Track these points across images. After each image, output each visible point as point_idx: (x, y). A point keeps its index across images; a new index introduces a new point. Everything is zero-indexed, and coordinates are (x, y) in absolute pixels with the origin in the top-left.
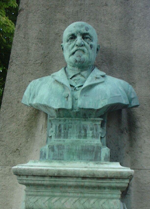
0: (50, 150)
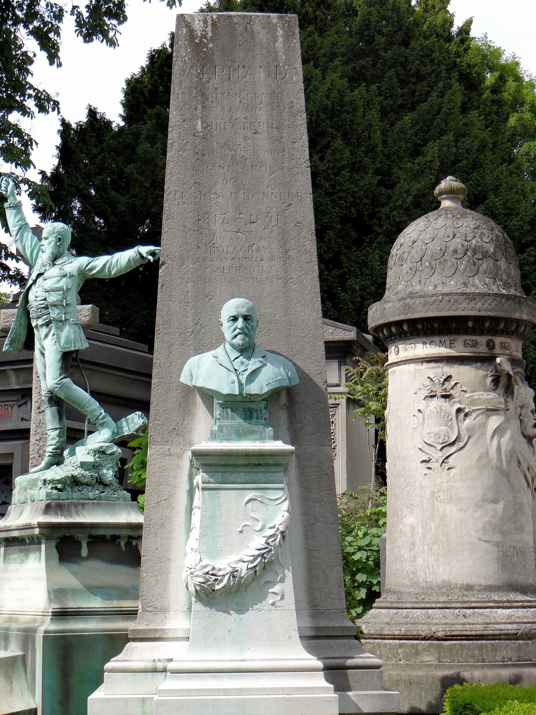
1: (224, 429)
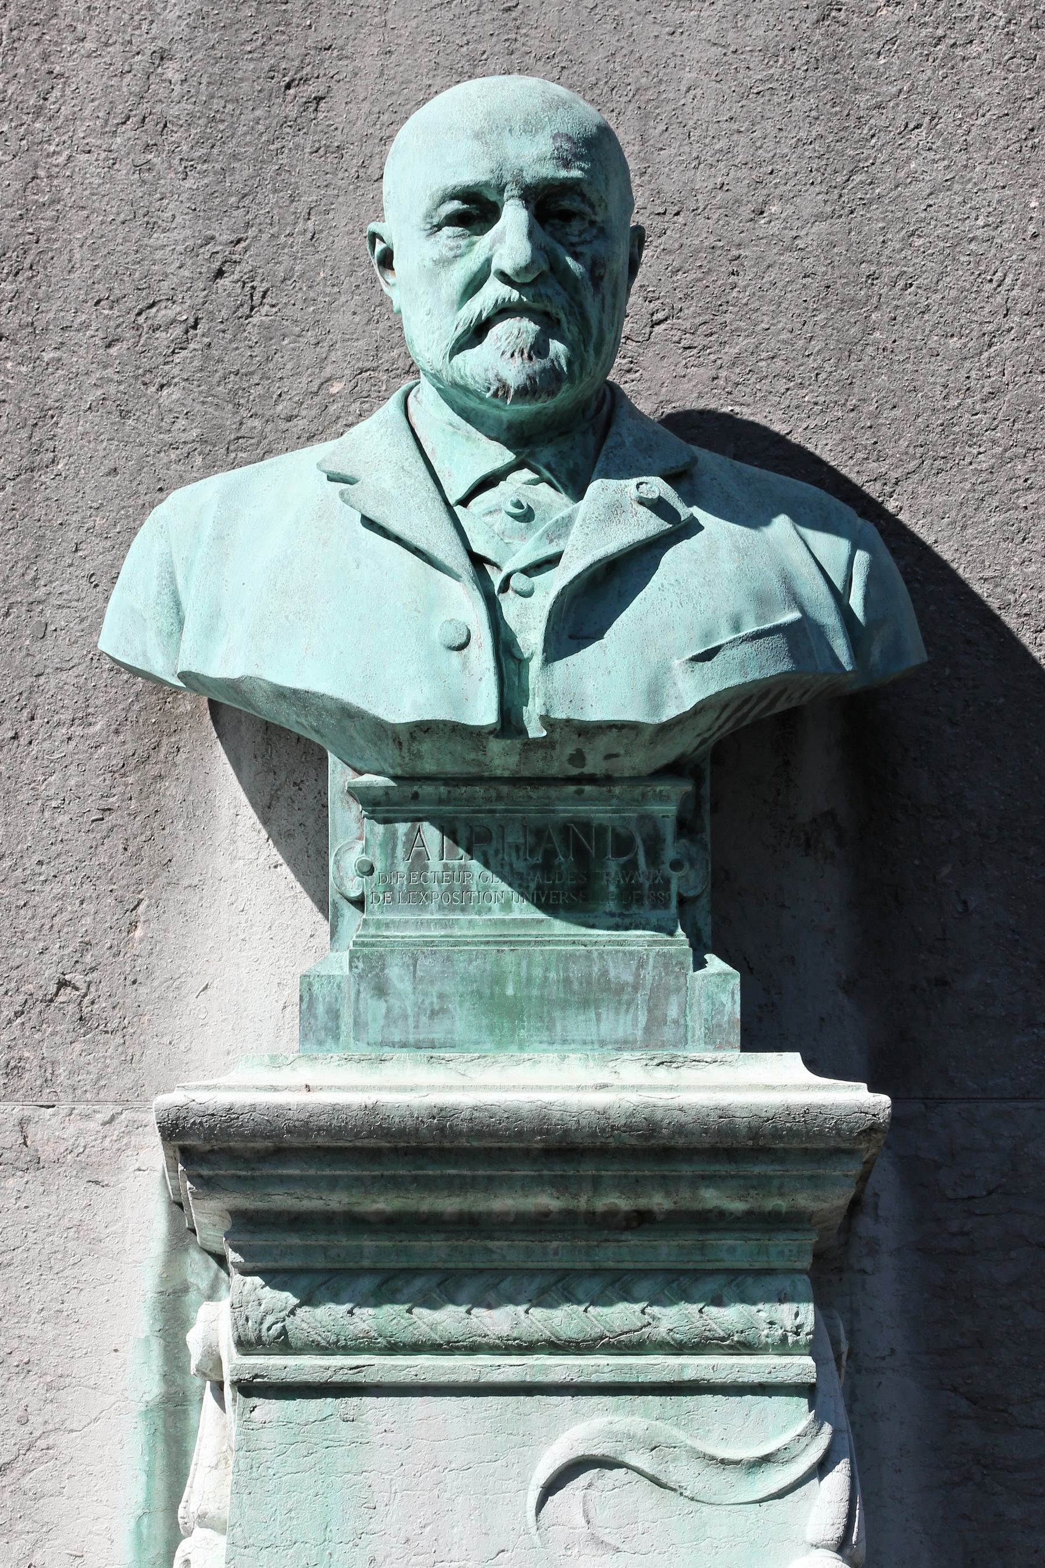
0: (363, 985)
1: (396, 973)
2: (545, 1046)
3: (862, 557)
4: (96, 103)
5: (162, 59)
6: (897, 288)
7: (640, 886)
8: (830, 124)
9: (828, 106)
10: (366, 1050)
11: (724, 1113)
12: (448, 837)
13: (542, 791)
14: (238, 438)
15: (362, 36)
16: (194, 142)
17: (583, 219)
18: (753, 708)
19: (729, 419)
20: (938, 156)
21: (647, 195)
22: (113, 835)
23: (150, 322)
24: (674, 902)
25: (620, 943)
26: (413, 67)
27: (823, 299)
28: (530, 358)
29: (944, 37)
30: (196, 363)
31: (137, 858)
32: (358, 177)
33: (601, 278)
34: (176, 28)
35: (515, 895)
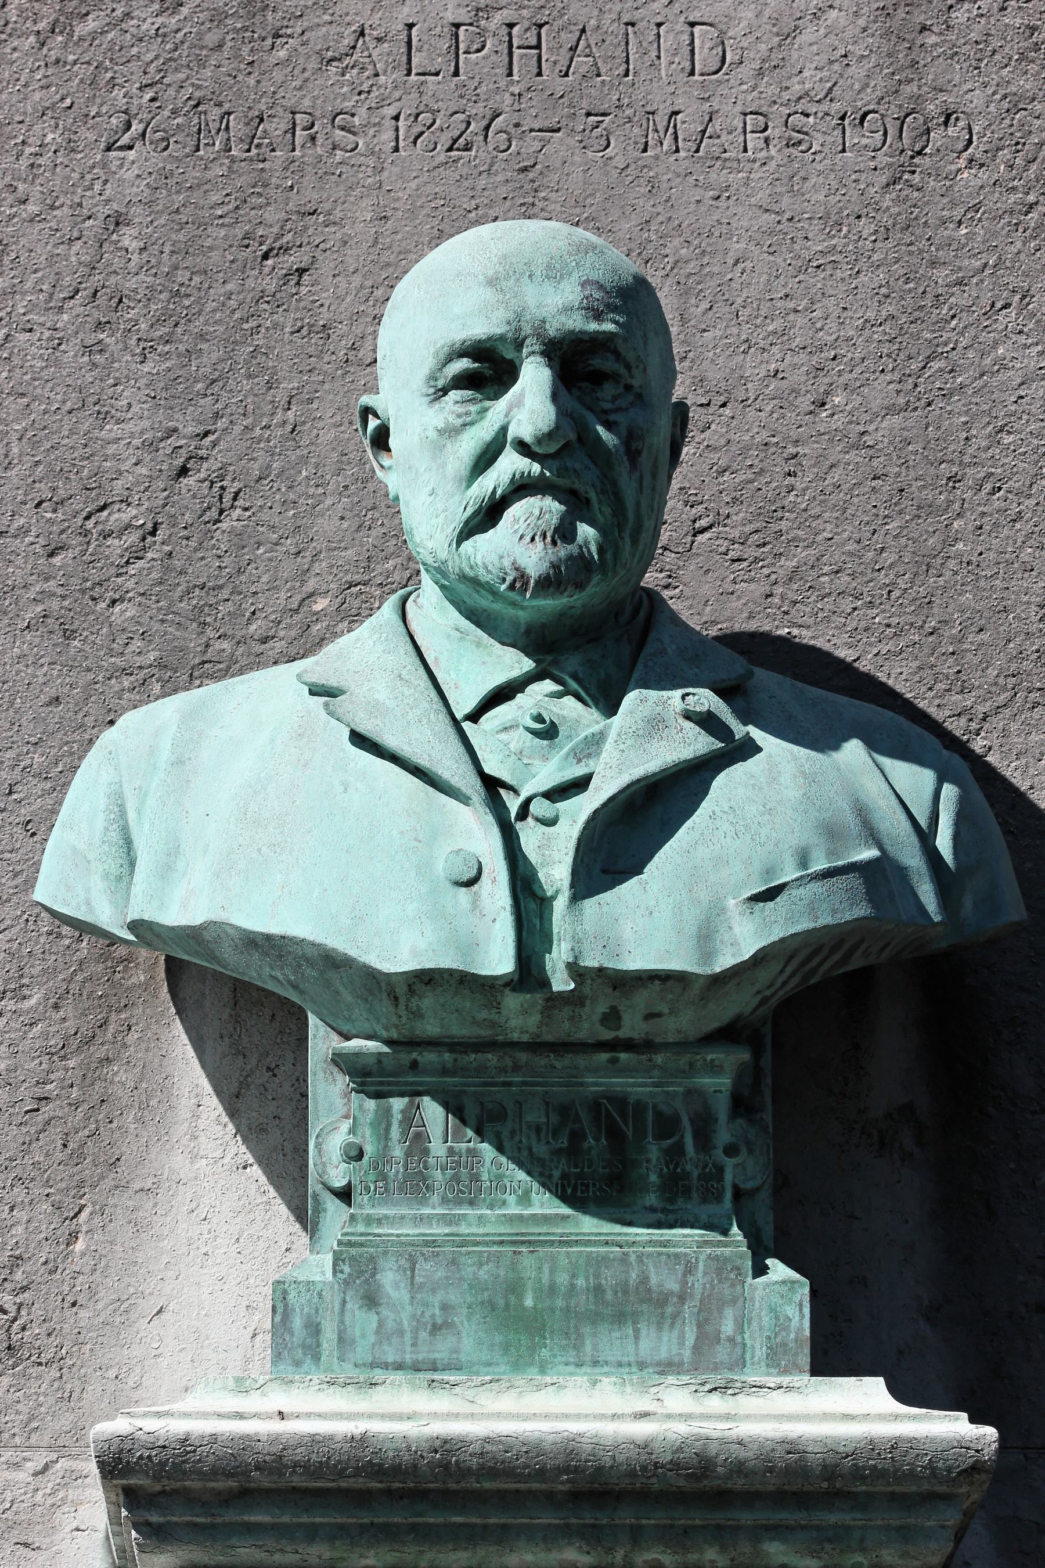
1: (389, 1278)
2: (571, 1368)
3: (949, 791)
4: (39, 274)
5: (117, 224)
6: (984, 492)
7: (687, 1175)
8: (903, 303)
9: (900, 282)
10: (354, 1373)
11: (792, 1446)
12: (454, 1115)
13: (568, 1059)
14: (204, 663)
15: (352, 199)
16: (154, 320)
17: (618, 382)
18: (824, 960)
19: (786, 642)
20: (1030, 341)
21: (687, 382)
22: (50, 1129)
23: (100, 527)
24: (728, 1195)
25: (664, 1244)
26: (413, 235)
27: (896, 504)
28: (554, 543)
29: (1036, 203)
30: (155, 575)
31: (79, 1156)
32: (347, 361)
33: (639, 453)
34: (135, 189)
35: (536, 1185)
